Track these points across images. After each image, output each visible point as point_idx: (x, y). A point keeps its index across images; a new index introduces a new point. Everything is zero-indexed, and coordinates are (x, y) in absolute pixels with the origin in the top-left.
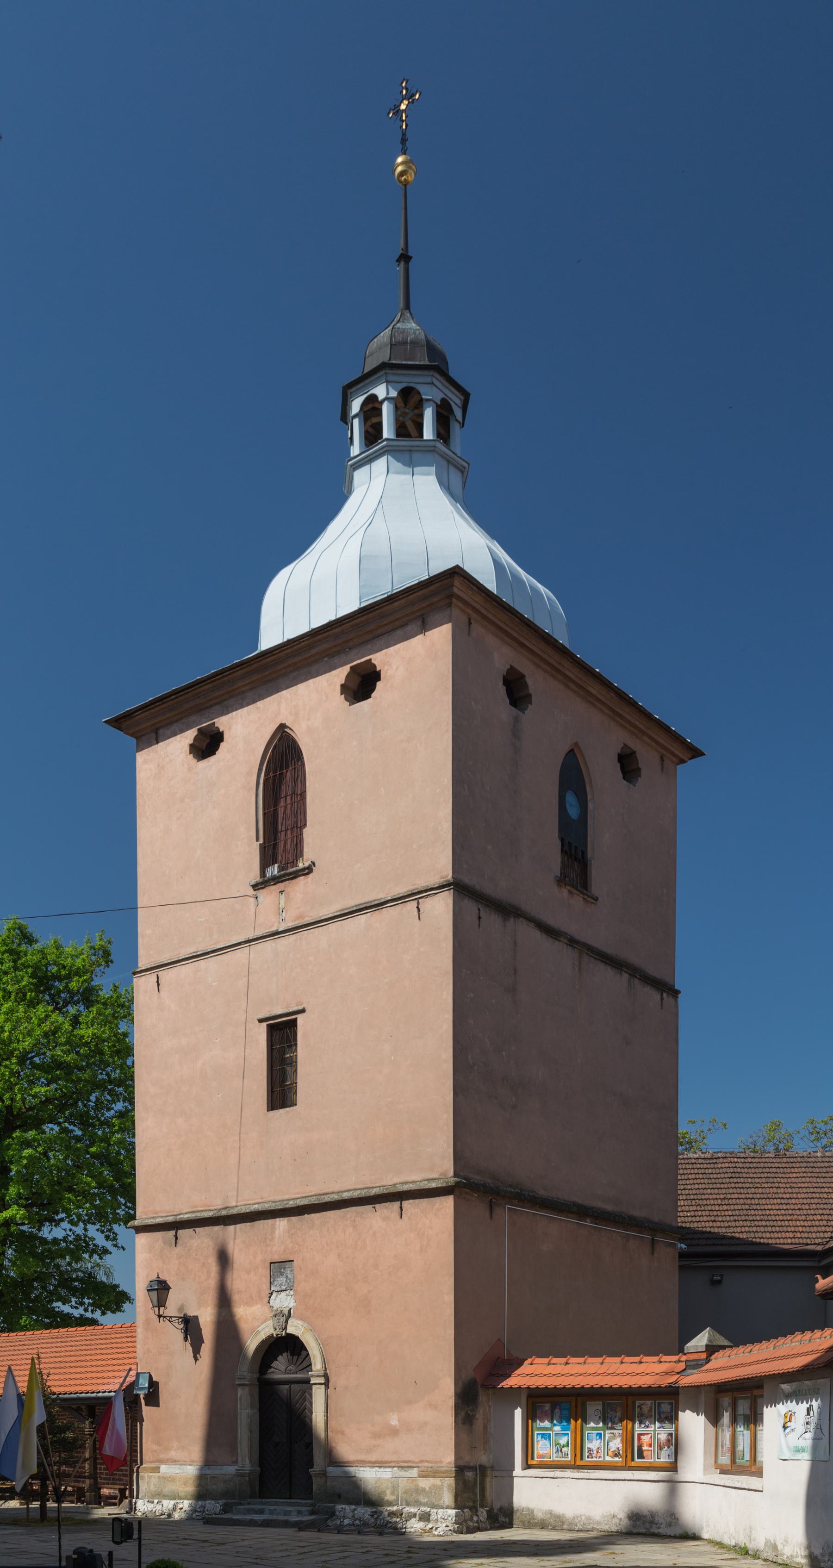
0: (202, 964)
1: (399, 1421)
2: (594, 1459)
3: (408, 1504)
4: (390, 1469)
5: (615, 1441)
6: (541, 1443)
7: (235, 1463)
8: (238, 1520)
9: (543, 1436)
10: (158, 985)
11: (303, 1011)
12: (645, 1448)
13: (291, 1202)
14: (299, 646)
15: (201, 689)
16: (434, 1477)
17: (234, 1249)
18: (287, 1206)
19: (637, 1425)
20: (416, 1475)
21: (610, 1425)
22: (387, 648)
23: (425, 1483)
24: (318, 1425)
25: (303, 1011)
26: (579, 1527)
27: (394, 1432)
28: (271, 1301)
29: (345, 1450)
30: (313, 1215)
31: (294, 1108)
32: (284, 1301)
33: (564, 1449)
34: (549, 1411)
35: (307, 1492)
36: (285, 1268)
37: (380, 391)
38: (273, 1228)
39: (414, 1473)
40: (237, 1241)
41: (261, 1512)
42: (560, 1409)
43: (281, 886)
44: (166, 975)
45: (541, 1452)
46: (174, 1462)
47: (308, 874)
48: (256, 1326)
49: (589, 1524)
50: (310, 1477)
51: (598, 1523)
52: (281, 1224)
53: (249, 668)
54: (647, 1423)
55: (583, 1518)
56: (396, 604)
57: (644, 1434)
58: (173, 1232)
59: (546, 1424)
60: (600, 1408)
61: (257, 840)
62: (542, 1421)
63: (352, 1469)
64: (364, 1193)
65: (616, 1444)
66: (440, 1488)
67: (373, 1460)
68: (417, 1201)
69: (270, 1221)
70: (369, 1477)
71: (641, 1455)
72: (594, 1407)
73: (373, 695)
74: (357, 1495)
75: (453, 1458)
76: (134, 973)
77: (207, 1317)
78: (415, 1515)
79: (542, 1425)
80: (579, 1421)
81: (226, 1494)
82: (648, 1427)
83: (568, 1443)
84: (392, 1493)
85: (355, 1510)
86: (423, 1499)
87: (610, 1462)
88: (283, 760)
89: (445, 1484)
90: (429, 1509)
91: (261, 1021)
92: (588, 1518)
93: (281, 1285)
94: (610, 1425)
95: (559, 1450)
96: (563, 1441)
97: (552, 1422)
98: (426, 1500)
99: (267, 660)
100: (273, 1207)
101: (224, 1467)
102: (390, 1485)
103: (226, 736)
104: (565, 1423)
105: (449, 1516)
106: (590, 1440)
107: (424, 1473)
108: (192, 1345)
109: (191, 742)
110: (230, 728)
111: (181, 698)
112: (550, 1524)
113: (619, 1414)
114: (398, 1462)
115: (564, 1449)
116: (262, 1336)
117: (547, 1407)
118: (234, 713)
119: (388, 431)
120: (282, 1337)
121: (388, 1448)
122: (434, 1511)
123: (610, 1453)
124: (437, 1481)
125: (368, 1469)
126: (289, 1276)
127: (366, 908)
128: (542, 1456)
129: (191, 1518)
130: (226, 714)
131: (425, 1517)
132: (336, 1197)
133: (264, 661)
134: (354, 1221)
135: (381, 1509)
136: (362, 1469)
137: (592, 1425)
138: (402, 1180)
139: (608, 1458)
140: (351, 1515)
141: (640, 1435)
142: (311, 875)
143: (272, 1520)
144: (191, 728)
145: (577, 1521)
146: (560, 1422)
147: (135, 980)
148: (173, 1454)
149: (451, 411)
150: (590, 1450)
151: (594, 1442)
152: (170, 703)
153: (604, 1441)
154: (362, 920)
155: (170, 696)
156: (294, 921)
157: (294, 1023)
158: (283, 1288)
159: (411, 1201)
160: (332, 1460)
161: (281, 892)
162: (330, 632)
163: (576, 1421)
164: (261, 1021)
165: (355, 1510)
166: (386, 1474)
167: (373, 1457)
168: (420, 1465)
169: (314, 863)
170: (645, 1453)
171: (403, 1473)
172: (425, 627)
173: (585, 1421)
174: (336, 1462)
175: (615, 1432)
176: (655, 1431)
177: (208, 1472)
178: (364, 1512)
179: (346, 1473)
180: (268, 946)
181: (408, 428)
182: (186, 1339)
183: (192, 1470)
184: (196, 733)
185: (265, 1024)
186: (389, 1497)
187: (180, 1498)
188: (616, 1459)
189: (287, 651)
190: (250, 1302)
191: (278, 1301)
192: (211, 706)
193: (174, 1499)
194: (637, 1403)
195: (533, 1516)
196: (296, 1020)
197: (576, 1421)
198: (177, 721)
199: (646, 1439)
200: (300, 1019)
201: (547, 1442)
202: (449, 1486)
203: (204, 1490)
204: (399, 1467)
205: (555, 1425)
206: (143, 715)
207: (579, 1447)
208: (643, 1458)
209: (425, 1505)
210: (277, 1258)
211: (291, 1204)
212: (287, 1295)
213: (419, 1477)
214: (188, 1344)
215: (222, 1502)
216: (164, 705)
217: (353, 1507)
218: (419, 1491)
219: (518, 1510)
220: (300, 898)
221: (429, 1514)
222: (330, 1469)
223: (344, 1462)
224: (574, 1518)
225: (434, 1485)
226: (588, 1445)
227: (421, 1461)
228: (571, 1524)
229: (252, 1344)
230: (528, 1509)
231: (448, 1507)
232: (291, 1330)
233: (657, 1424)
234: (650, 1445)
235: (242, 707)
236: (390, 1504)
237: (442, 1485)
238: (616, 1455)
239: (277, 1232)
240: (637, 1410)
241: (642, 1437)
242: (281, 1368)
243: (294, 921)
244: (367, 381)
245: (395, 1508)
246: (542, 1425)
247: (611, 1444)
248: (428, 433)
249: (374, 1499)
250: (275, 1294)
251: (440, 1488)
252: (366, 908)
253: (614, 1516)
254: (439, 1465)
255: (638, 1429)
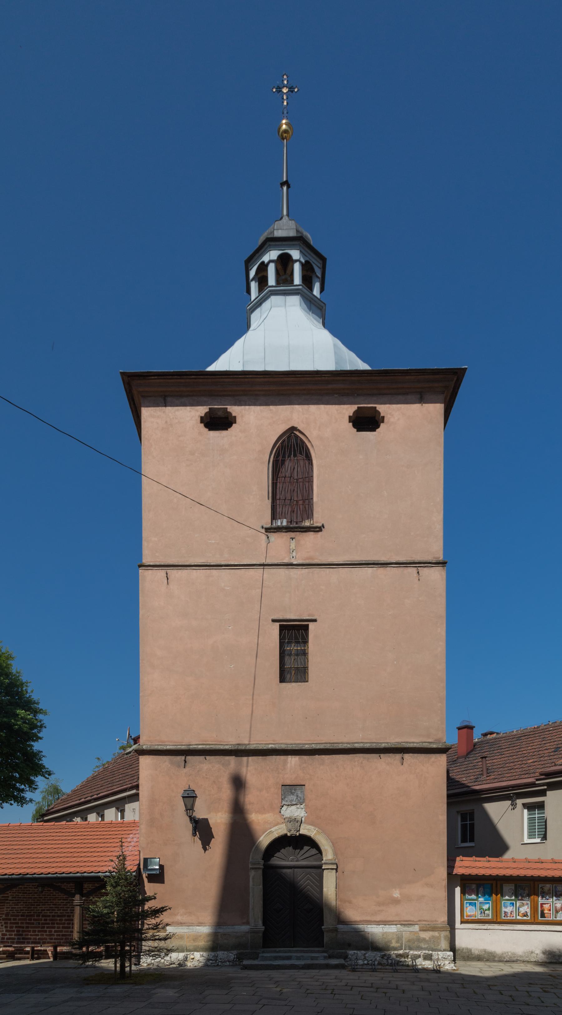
0: (215, 572)
1: (400, 894)
2: (509, 918)
3: (411, 949)
4: (395, 926)
5: (524, 908)
6: (469, 908)
7: (248, 923)
8: (278, 965)
9: (470, 904)
10: (168, 579)
11: (315, 621)
12: (546, 911)
13: (307, 746)
14: (319, 378)
15: (222, 380)
16: (433, 931)
17: (247, 773)
18: (304, 748)
19: (540, 898)
20: (418, 930)
21: (520, 898)
22: (390, 404)
23: (426, 935)
24: (329, 897)
25: (315, 621)
26: (507, 959)
27: (396, 902)
28: (282, 812)
29: (352, 914)
30: (323, 756)
31: (306, 683)
32: (297, 812)
33: (486, 912)
34: (475, 889)
35: (320, 943)
36: (295, 790)
37: (295, 254)
38: (285, 762)
39: (416, 928)
40: (249, 768)
41: (289, 958)
42: (484, 888)
43: (292, 534)
44: (174, 574)
45: (469, 914)
46: (181, 924)
47: (318, 531)
48: (268, 827)
49: (514, 957)
50: (322, 933)
51: (521, 956)
52: (293, 760)
53: (271, 380)
54: (547, 897)
55: (510, 954)
56: (407, 377)
57: (545, 904)
58: (183, 758)
59: (473, 897)
60: (513, 888)
61: (268, 499)
62: (470, 895)
63: (361, 926)
64: (374, 746)
65: (526, 908)
66: (439, 938)
67: (378, 920)
68: (416, 755)
69: (282, 758)
70: (376, 931)
71: (543, 915)
72: (507, 887)
73: (377, 430)
74: (366, 944)
75: (446, 919)
76: (140, 566)
77: (219, 820)
78: (419, 956)
79: (470, 897)
80: (499, 895)
81: (236, 947)
82: (548, 899)
83: (489, 908)
84: (397, 942)
85: (365, 954)
86: (423, 945)
87: (519, 920)
88: (291, 451)
89: (442, 935)
90: (431, 952)
91: (274, 621)
92: (514, 954)
93: (292, 801)
94: (520, 898)
95: (483, 912)
96: (486, 907)
97: (477, 895)
98: (426, 946)
99: (288, 379)
100: (290, 747)
101: (236, 927)
102: (395, 936)
103: (238, 420)
104: (487, 896)
105: (449, 956)
106: (506, 907)
107: (424, 928)
108: (200, 839)
109: (203, 415)
110: (242, 416)
111: (201, 380)
112: (484, 958)
113: (526, 892)
114: (400, 921)
115: (486, 912)
116: (275, 835)
117: (474, 886)
118: (247, 407)
119: (272, 280)
120: (296, 836)
121: (391, 912)
122: (434, 953)
123: (520, 914)
124: (436, 934)
125: (375, 926)
126: (300, 795)
127: (374, 564)
128: (470, 916)
129: (209, 964)
130: (238, 405)
131: (428, 957)
132: (349, 746)
133: (286, 379)
134: (362, 763)
135: (388, 953)
136: (369, 926)
137: (507, 897)
138: (403, 741)
139: (519, 918)
140: (363, 957)
141: (542, 904)
142: (320, 533)
143: (312, 964)
144: (207, 406)
145: (505, 955)
146: (484, 895)
147: (140, 571)
148: (179, 918)
149: (313, 270)
150: (505, 913)
151: (509, 908)
152: (187, 380)
153: (512, 907)
154: (369, 571)
155: (191, 375)
156: (305, 560)
157: (306, 628)
158: (294, 803)
159: (411, 755)
160: (340, 920)
161: (292, 539)
162: (349, 378)
163: (497, 895)
164: (274, 621)
165: (365, 954)
166: (392, 929)
167: (378, 918)
168: (419, 923)
169: (323, 526)
170: (546, 915)
171: (406, 929)
172: (422, 400)
173: (502, 896)
174: (344, 922)
175: (523, 902)
176: (553, 902)
177: (221, 930)
178: (377, 956)
179: (354, 929)
180: (282, 572)
181: (284, 274)
182: (194, 834)
183: (205, 930)
184: (207, 410)
185: (277, 624)
186: (394, 944)
187: (190, 951)
188: (525, 918)
189: (308, 379)
190: (262, 810)
191: (288, 811)
192: (224, 396)
193: (182, 951)
194: (540, 886)
195: (471, 953)
196: (308, 626)
197: (497, 895)
198: (187, 396)
199: (546, 907)
200: (312, 626)
201: (474, 908)
202: (445, 937)
203: (216, 945)
204: (401, 925)
205: (480, 897)
206: (158, 381)
207: (497, 910)
208: (545, 917)
209: (425, 949)
210: (288, 782)
211: (307, 747)
212: (298, 808)
213: (420, 930)
214: (197, 839)
215: (235, 952)
216: (182, 381)
217: (363, 952)
218: (419, 940)
219: (459, 950)
220: (306, 546)
221: (431, 955)
222: (340, 926)
223: (351, 922)
224: (503, 954)
225: (433, 936)
226: (504, 909)
227: (420, 921)
228: (500, 957)
229: (264, 840)
230: (467, 949)
231: (444, 950)
232: (302, 832)
233: (554, 898)
234: (550, 910)
235: (255, 404)
236: (395, 949)
237: (440, 936)
238: (525, 916)
239: (289, 765)
240: (540, 890)
241: (544, 905)
242: (285, 859)
243: (305, 560)
244: (260, 252)
245: (401, 952)
246: (470, 897)
247: (521, 909)
248: (297, 279)
249: (381, 946)
250: (285, 807)
251: (439, 938)
252: (374, 564)
253: (532, 952)
254: (435, 923)
255: (540, 900)
